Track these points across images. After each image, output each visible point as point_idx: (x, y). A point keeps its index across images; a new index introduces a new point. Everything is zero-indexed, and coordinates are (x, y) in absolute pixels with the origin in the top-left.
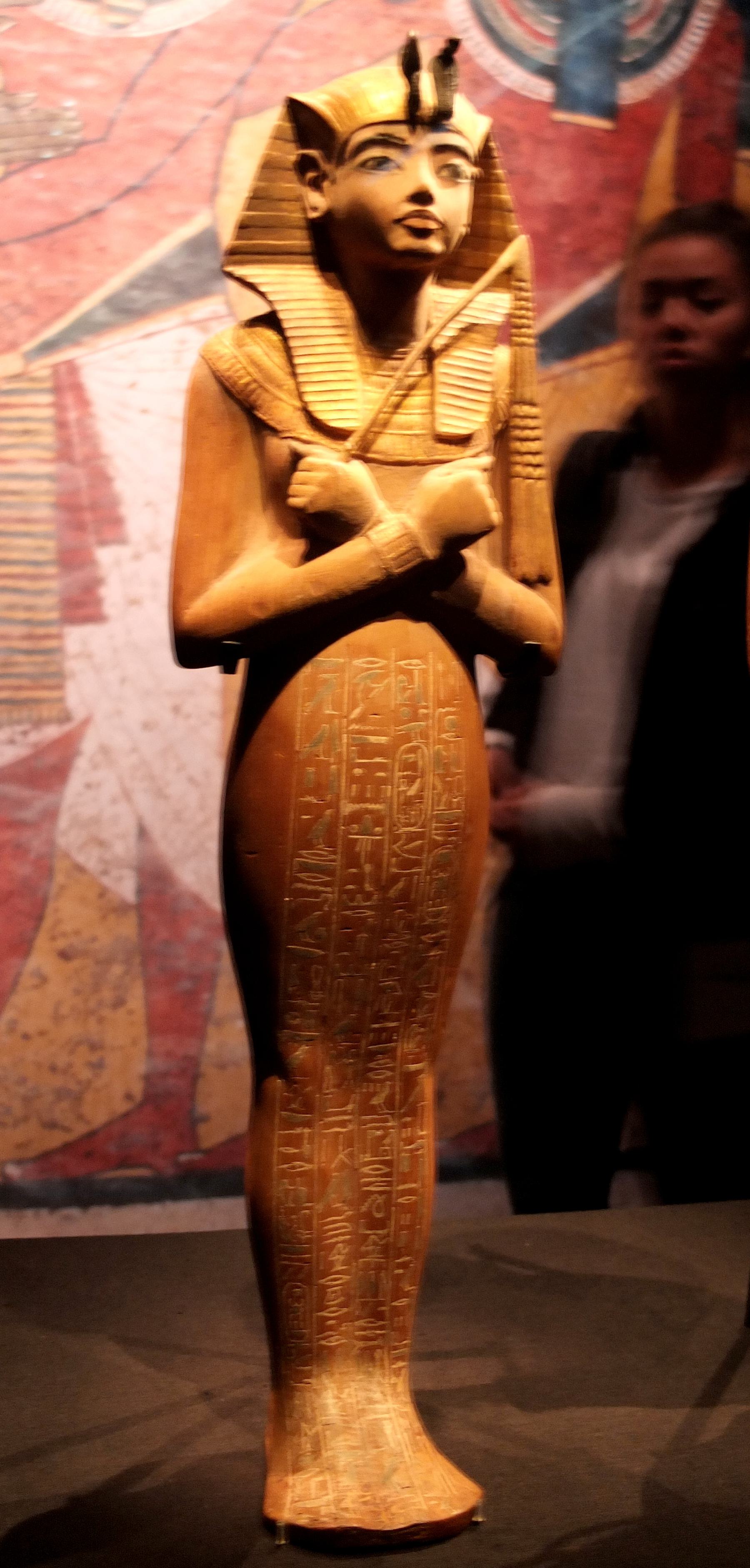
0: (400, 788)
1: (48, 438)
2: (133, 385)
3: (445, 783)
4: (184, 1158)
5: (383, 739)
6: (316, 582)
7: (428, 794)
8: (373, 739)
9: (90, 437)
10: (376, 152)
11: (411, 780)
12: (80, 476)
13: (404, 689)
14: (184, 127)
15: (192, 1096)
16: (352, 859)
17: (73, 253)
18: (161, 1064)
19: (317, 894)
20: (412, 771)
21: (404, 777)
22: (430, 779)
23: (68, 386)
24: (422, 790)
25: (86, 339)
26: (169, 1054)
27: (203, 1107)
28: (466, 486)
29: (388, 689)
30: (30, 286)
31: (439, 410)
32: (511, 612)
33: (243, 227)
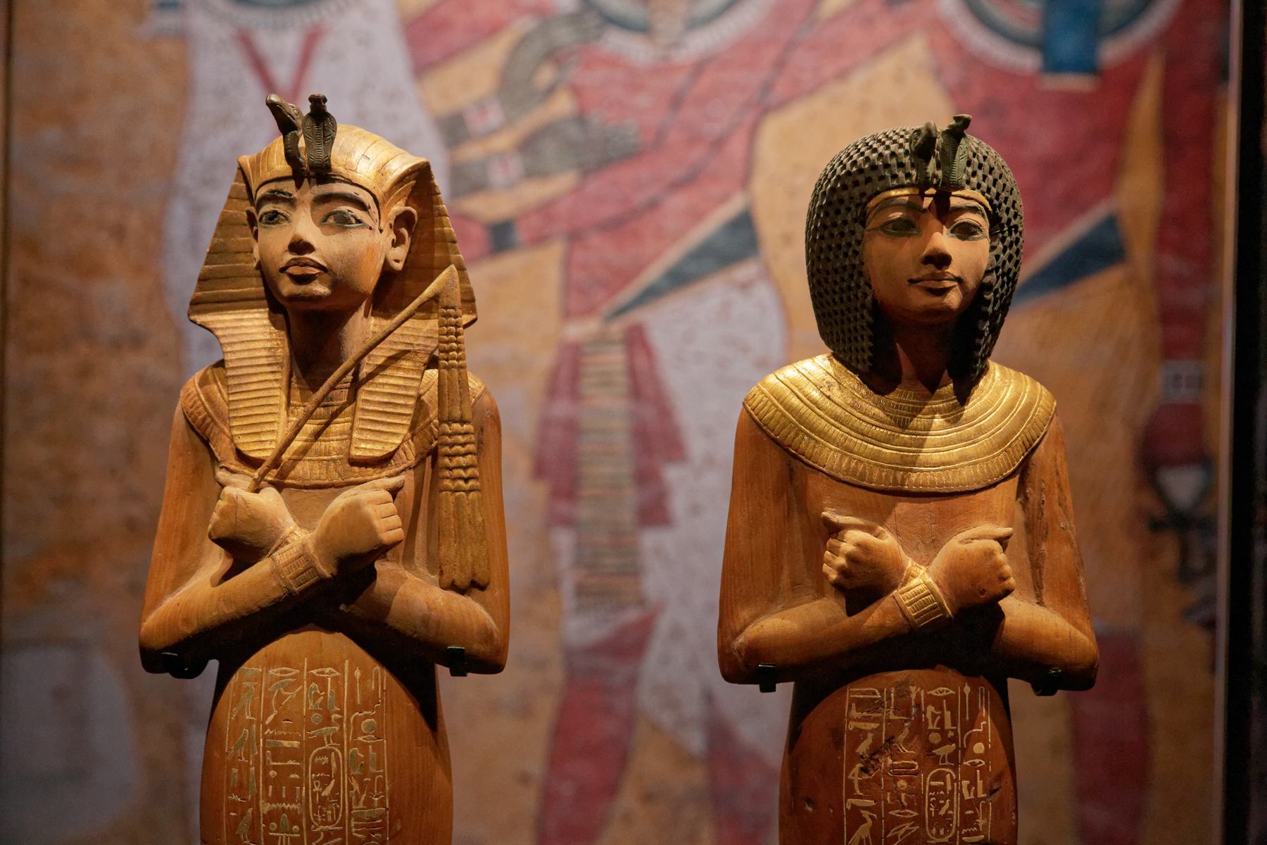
1: (622, 380)
3: (361, 784)
5: (296, 744)
6: (228, 601)
7: (344, 794)
8: (286, 743)
9: (656, 381)
10: (268, 208)
11: (324, 782)
12: (649, 412)
13: (317, 696)
14: (715, 129)
21: (316, 778)
22: (344, 780)
23: (636, 340)
28: (354, 508)
29: (300, 695)
31: (355, 435)
32: (426, 621)
33: (203, 279)
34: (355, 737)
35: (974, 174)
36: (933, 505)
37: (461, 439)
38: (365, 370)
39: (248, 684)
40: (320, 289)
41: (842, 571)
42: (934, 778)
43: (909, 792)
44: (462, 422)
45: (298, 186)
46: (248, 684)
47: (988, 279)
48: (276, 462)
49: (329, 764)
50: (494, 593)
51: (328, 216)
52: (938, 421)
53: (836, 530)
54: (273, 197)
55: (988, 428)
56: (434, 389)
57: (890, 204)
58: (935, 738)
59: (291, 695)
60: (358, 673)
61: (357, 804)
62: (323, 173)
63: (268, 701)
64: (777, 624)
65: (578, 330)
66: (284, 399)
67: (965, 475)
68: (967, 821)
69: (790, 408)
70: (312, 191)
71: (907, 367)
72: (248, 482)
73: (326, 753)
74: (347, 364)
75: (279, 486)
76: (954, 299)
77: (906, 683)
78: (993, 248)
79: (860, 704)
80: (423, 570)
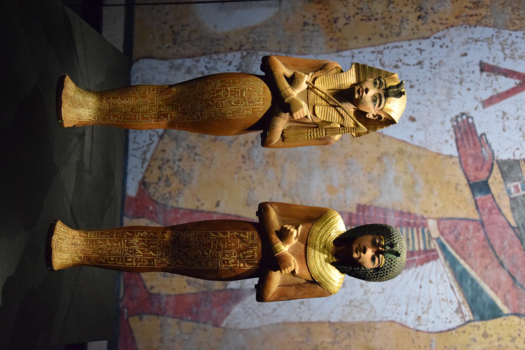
0: (233, 100)
2: (431, 282)
3: (234, 112)
4: (126, 310)
7: (232, 107)
8: (244, 93)
10: (378, 82)
11: (235, 103)
15: (150, 313)
16: (218, 91)
17: (483, 256)
18: (164, 300)
20: (237, 103)
22: (235, 107)
24: (234, 106)
25: (448, 263)
26: (167, 303)
27: (145, 317)
29: (256, 96)
30: (467, 239)
32: (274, 126)
35: (389, 262)
36: (303, 254)
37: (321, 134)
38: (339, 109)
40: (357, 96)
41: (286, 228)
42: (235, 253)
43: (231, 246)
44: (325, 134)
45: (384, 89)
47: (363, 268)
48: (314, 87)
50: (282, 143)
52: (326, 256)
53: (297, 228)
54: (381, 83)
55: (324, 270)
56: (335, 126)
57: (381, 239)
58: (244, 253)
59: (256, 93)
60: (261, 109)
62: (387, 96)
63: (254, 88)
64: (273, 215)
65: (432, 224)
66: (331, 88)
67: (311, 263)
68: (224, 262)
69: (330, 219)
70: (382, 93)
71: (340, 248)
72: (308, 81)
73: (242, 103)
74: (340, 104)
75: (308, 88)
76: (355, 256)
77: (258, 246)
78: (371, 269)
79: (253, 235)
80: (287, 125)
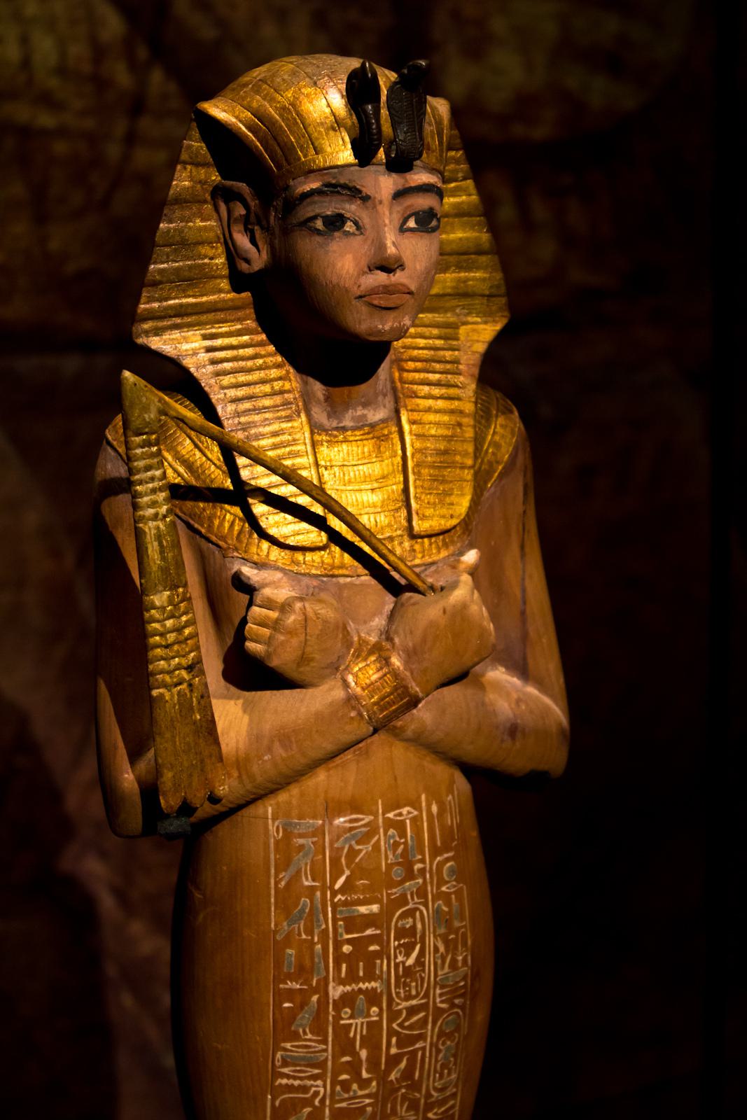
3: (447, 942)
5: (375, 908)
7: (429, 959)
8: (363, 909)
11: (408, 949)
13: (396, 845)
16: (345, 1044)
19: (305, 1089)
22: (430, 941)
34: (439, 887)
39: (301, 841)
46: (301, 841)
49: (414, 927)
51: (406, 220)
59: (365, 849)
60: (434, 808)
61: (443, 968)
73: (411, 913)
